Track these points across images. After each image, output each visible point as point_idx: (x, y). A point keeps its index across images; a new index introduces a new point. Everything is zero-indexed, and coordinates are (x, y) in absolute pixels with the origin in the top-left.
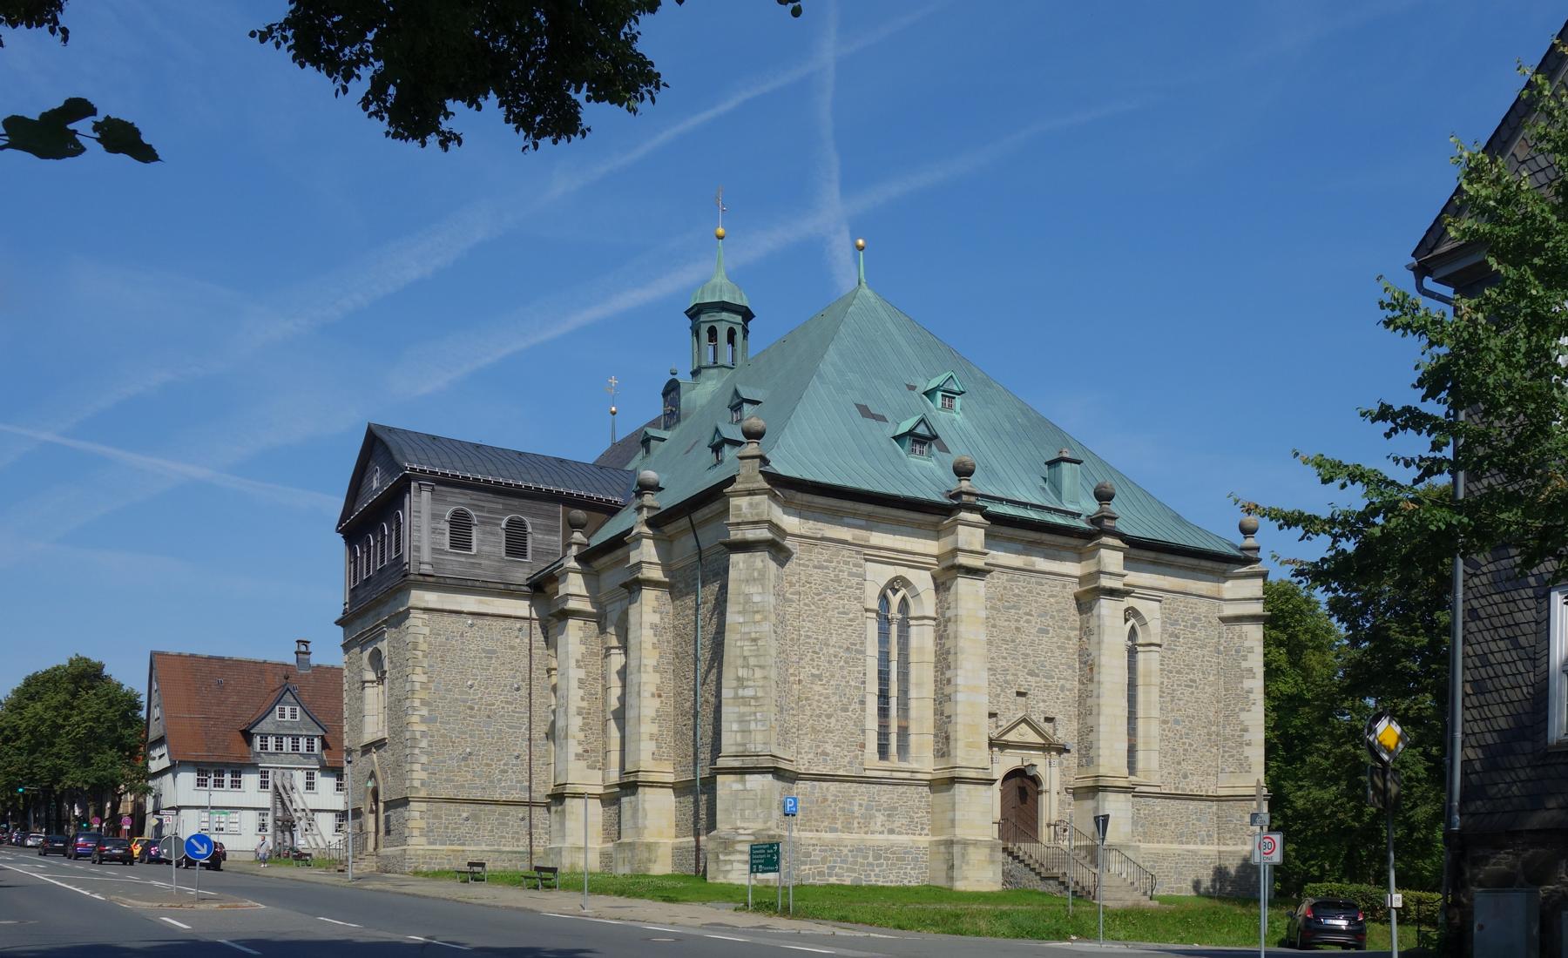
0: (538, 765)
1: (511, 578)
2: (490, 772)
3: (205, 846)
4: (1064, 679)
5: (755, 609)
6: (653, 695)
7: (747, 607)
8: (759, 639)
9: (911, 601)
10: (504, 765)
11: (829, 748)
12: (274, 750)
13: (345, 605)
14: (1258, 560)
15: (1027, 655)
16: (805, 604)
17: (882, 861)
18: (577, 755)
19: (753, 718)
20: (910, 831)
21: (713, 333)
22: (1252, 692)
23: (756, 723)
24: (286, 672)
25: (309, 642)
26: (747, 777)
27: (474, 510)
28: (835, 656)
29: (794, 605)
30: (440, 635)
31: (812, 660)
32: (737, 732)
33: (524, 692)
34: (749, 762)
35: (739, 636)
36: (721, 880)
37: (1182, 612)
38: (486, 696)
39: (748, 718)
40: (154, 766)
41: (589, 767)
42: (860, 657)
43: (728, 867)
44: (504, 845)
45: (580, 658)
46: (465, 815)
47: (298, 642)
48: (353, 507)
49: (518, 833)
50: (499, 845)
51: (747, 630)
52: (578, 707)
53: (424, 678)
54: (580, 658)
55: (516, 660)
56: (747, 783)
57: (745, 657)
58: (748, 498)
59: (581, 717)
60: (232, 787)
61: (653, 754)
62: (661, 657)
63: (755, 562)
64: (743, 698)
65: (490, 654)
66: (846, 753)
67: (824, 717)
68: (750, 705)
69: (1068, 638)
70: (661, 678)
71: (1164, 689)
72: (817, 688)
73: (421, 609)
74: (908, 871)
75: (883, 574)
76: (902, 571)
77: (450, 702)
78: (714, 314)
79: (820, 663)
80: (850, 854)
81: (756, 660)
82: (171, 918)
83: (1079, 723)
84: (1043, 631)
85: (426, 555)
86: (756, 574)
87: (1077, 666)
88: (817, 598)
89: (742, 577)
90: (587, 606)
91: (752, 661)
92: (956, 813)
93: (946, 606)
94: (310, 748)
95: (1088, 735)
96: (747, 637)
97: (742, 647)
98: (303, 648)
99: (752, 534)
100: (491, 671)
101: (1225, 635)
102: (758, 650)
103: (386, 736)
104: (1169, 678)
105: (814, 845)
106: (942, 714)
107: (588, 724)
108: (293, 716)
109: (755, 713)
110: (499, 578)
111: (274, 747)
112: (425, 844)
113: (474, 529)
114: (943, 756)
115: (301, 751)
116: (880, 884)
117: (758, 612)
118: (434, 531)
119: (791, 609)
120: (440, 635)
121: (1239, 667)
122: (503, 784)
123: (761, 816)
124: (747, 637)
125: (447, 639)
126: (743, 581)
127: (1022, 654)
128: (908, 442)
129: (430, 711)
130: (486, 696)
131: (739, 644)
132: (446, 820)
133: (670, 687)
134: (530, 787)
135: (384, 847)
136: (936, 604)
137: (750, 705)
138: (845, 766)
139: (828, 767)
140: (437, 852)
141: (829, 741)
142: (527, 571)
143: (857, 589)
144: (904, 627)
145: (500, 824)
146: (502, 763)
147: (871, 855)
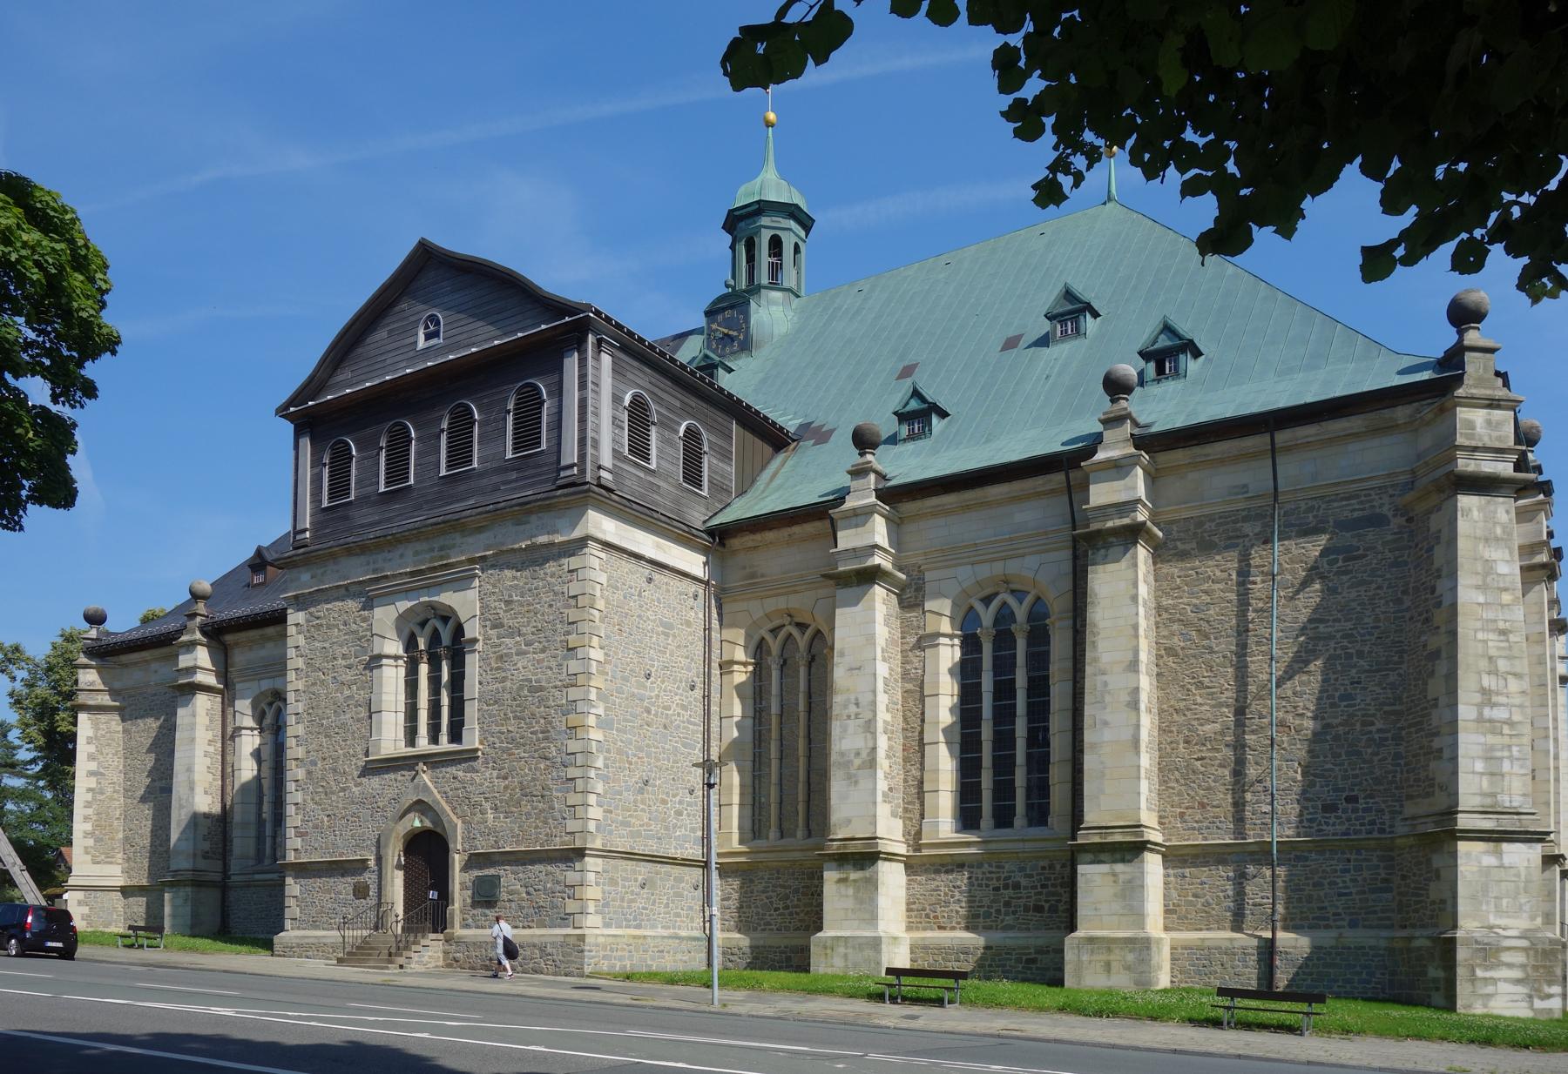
2: (665, 813)
5: (1502, 585)
7: (1489, 579)
8: (1511, 632)
23: (1512, 762)
26: (1505, 846)
32: (1482, 774)
34: (1508, 823)
35: (1479, 624)
36: (1479, 1010)
39: (1499, 754)
43: (1490, 989)
51: (1491, 615)
56: (1504, 856)
57: (1490, 658)
63: (1495, 512)
64: (1491, 721)
78: (781, 219)
82: (238, 1062)
86: (1499, 531)
89: (1479, 533)
91: (1502, 665)
96: (1491, 626)
97: (1485, 642)
102: (1510, 648)
103: (477, 745)
109: (1510, 746)
112: (600, 925)
113: (653, 430)
117: (1506, 590)
122: (678, 833)
123: (1526, 908)
124: (1491, 626)
126: (1480, 539)
131: (1480, 636)
132: (624, 887)
140: (619, 940)
146: (678, 798)
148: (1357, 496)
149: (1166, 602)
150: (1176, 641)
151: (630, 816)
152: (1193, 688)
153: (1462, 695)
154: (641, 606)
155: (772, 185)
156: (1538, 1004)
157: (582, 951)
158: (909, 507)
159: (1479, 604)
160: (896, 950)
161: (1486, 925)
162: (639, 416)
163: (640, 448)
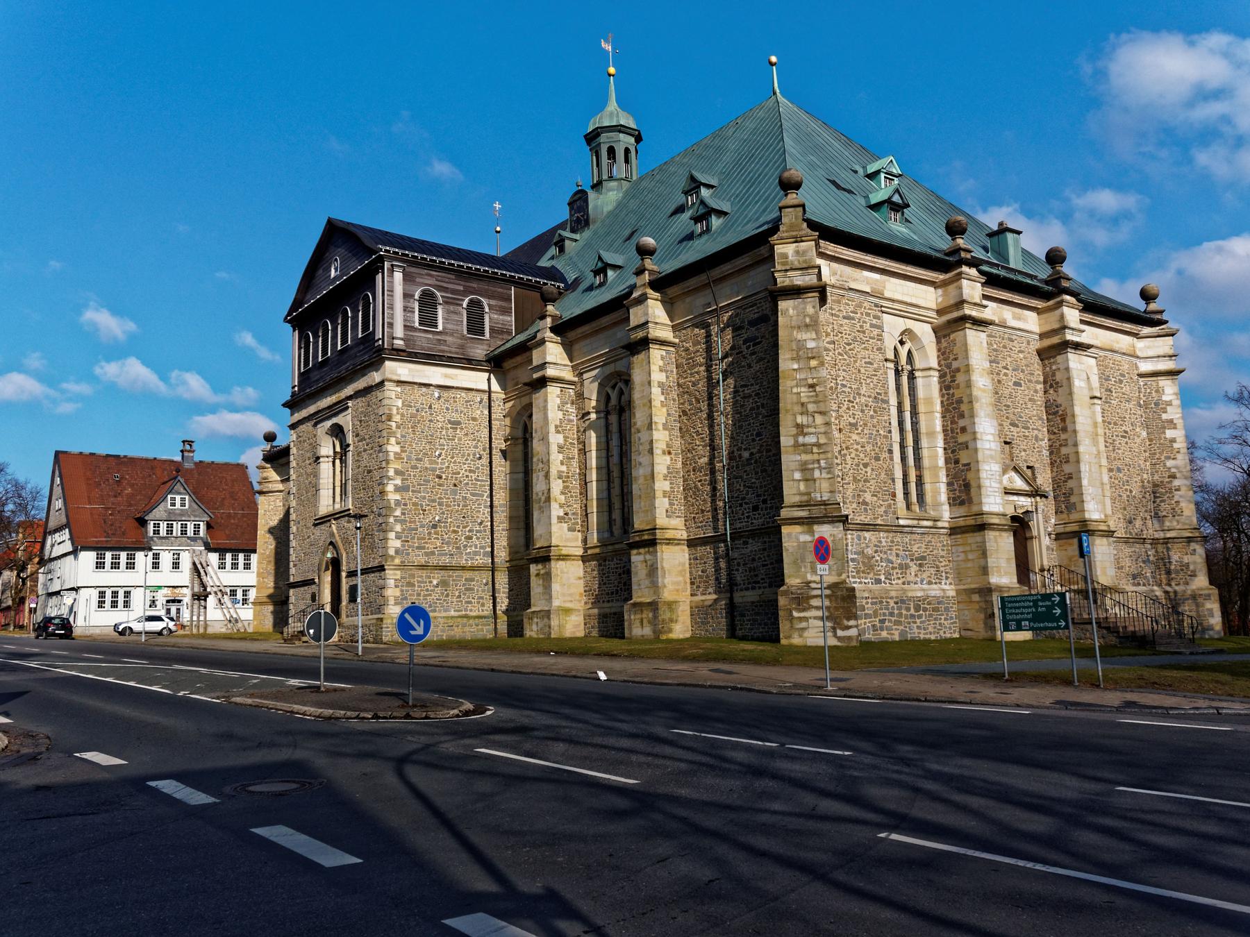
0: (498, 530)
1: (472, 354)
3: (422, 622)
4: (1037, 429)
5: (810, 355)
6: (664, 453)
9: (915, 353)
10: (470, 531)
11: (868, 497)
12: (165, 535)
13: (293, 387)
14: (1166, 322)
15: (1008, 406)
16: (839, 354)
17: (921, 612)
18: (559, 518)
19: (816, 465)
20: (937, 581)
21: (611, 152)
22: (1175, 442)
24: (177, 467)
25: (193, 442)
27: (438, 291)
28: (866, 406)
29: (831, 354)
30: (411, 407)
31: (848, 409)
32: (800, 480)
33: (485, 461)
34: (816, 512)
36: (796, 640)
37: (1111, 368)
38: (452, 465)
40: (58, 551)
41: (569, 530)
42: (885, 406)
43: (804, 625)
44: (471, 610)
45: (558, 423)
46: (435, 582)
47: (184, 442)
48: (304, 298)
49: (482, 598)
50: (466, 610)
51: (803, 376)
52: (558, 471)
53: (397, 449)
54: (558, 423)
55: (478, 431)
57: (803, 404)
58: (795, 244)
59: (561, 481)
60: (127, 568)
61: (667, 511)
62: (669, 415)
64: (804, 445)
65: (455, 424)
66: (882, 503)
67: (861, 466)
68: (812, 453)
69: (1036, 391)
70: (670, 435)
71: (1107, 440)
72: (855, 437)
73: (394, 381)
74: (942, 621)
75: (900, 324)
76: (911, 324)
77: (421, 472)
79: (855, 412)
80: (895, 606)
81: (815, 405)
83: (1052, 471)
84: (1017, 384)
85: (399, 331)
86: (808, 320)
87: (1045, 417)
88: (848, 348)
89: (794, 323)
90: (568, 375)
91: (811, 407)
92: (989, 560)
93: (952, 357)
94: (196, 532)
95: (1066, 482)
97: (799, 394)
98: (188, 447)
99: (799, 280)
100: (456, 441)
101: (1143, 390)
104: (1109, 429)
105: (866, 598)
106: (957, 462)
107: (568, 487)
108: (183, 505)
109: (818, 461)
110: (463, 354)
111: (165, 532)
114: (962, 503)
115: (188, 535)
116: (922, 636)
117: (813, 358)
118: (405, 309)
119: (828, 358)
120: (411, 407)
121: (1160, 419)
122: (468, 550)
125: (418, 411)
127: (1005, 406)
128: (885, 208)
129: (402, 480)
130: (452, 465)
131: (795, 390)
133: (678, 443)
134: (492, 552)
135: (347, 616)
136: (938, 357)
137: (812, 453)
138: (882, 516)
139: (869, 517)
141: (868, 490)
142: (486, 347)
143: (878, 340)
144: (912, 377)
145: (467, 589)
146: (467, 529)
147: (912, 606)
148: (756, 304)
149: (681, 381)
150: (687, 406)
151: (426, 543)
152: (694, 435)
153: (782, 431)
154: (431, 414)
155: (613, 113)
156: (840, 633)
157: (382, 628)
158: (572, 335)
159: (794, 370)
160: (568, 619)
161: (805, 581)
162: (428, 302)
163: (428, 320)
